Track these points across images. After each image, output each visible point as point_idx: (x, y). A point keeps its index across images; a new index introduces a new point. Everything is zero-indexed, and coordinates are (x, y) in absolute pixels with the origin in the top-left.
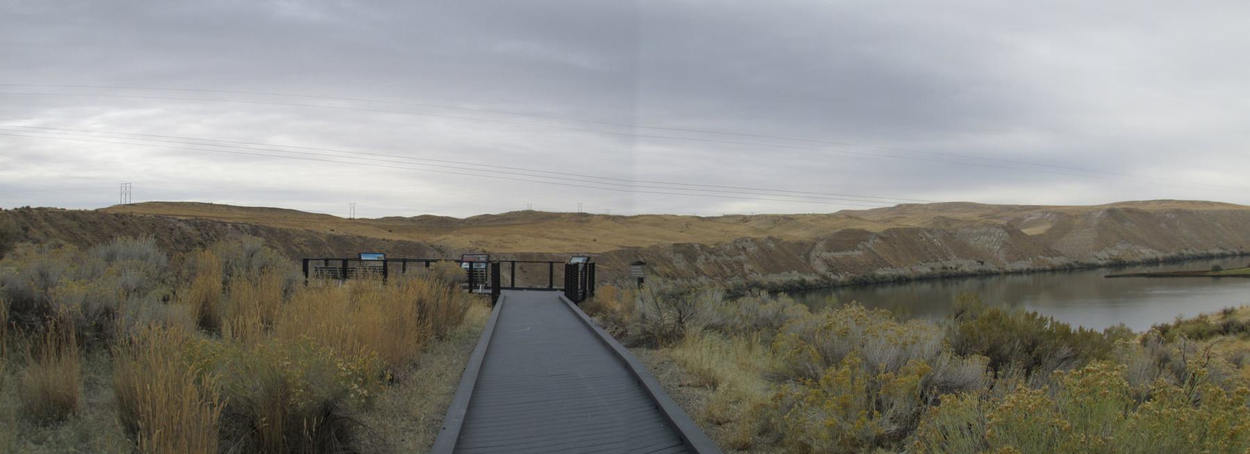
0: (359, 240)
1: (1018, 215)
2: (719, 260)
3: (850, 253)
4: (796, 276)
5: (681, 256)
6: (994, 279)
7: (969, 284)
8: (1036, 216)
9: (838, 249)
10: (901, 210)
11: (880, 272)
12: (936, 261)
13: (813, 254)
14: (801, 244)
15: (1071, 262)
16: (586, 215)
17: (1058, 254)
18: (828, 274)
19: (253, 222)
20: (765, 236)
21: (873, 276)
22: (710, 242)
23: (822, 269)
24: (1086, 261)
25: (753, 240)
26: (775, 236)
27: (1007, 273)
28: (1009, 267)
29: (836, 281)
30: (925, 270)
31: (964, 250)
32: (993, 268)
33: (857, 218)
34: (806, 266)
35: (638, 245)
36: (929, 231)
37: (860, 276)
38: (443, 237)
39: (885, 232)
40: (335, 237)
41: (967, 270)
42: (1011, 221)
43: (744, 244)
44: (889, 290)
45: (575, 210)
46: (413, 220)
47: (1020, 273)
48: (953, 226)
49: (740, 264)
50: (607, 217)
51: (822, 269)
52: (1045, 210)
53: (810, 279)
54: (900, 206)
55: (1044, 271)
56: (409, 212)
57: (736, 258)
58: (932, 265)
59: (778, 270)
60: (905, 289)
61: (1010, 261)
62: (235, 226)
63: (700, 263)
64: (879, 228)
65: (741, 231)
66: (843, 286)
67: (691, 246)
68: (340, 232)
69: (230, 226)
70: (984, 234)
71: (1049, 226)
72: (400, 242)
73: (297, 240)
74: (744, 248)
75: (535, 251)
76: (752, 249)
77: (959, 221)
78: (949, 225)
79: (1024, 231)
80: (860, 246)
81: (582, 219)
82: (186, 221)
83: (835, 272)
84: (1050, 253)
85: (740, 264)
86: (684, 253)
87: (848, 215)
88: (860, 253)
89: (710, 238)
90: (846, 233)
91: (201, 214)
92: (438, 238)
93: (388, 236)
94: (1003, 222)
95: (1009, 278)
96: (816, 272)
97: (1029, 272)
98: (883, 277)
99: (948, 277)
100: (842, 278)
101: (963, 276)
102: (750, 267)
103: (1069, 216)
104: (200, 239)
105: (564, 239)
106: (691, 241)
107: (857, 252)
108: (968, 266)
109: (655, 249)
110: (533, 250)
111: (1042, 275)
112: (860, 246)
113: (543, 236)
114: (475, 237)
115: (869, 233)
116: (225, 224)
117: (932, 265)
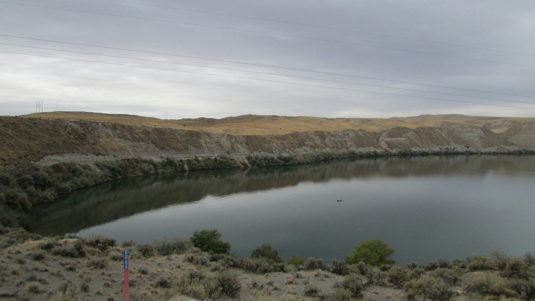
0: (168, 131)
1: (488, 122)
2: (336, 139)
3: (399, 139)
4: (372, 149)
5: (318, 137)
6: (474, 156)
7: (459, 158)
8: (499, 122)
9: (393, 137)
10: (423, 118)
11: (414, 149)
12: (443, 145)
13: (380, 138)
14: (375, 133)
15: (520, 149)
16: (276, 116)
17: (512, 145)
18: (388, 149)
19: (113, 122)
20: (358, 129)
21: (410, 151)
22: (332, 130)
23: (385, 146)
24: (530, 149)
25: (352, 130)
26: (363, 128)
27: (482, 154)
28: (483, 150)
29: (391, 153)
30: (436, 149)
31: (458, 140)
32: (474, 150)
33: (402, 121)
34: (377, 144)
35: (297, 131)
36: (440, 129)
37: (403, 151)
38: (209, 128)
39: (417, 128)
40: (156, 129)
41: (460, 150)
42: (485, 125)
43: (348, 132)
44: (417, 159)
45: (271, 114)
46: (195, 120)
47: (489, 154)
48: (453, 127)
49: (346, 142)
50: (286, 117)
51: (385, 146)
52: (505, 120)
53: (379, 151)
54: (422, 115)
55: (504, 154)
56: (194, 116)
57: (344, 139)
58: (441, 147)
59: (363, 146)
60: (425, 159)
61: (484, 147)
62: (103, 124)
63: (327, 141)
64: (413, 127)
65: (346, 126)
66: (395, 155)
67: (323, 132)
68: (159, 126)
69: (100, 124)
70: (470, 132)
71: (506, 129)
72: (189, 131)
73: (137, 131)
74: (348, 134)
75: (252, 134)
76: (352, 135)
77: (455, 124)
78: (450, 127)
79: (493, 131)
80: (404, 135)
81: (274, 118)
82: (75, 122)
83: (391, 148)
84: (507, 143)
85: (346, 142)
86: (320, 135)
87: (398, 120)
88: (404, 139)
89: (332, 128)
90: (397, 129)
91: (84, 118)
92: (207, 129)
93: (183, 128)
94: (481, 126)
95: (483, 156)
96: (382, 148)
97: (495, 154)
98: (415, 152)
99: (448, 154)
100: (394, 151)
101: (457, 154)
102: (350, 144)
103: (519, 123)
104: (83, 132)
105: (266, 128)
106: (322, 130)
107: (402, 139)
108: (460, 148)
109: (306, 133)
110: (252, 134)
111: (502, 156)
112: (404, 135)
113: (256, 127)
114: (225, 128)
115: (409, 129)
116: (97, 123)
117: (441, 147)
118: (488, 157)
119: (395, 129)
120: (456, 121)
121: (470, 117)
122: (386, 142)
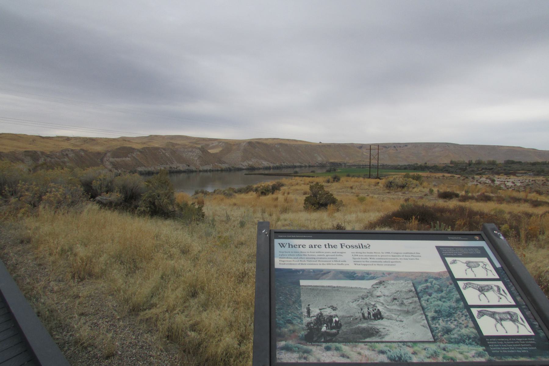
3: (124, 159)
6: (194, 174)
7: (182, 175)
8: (216, 143)
10: (152, 138)
13: (105, 159)
14: (99, 153)
17: (224, 163)
25: (72, 150)
26: (85, 149)
27: (200, 171)
42: (203, 145)
47: (206, 171)
48: (176, 147)
55: (218, 171)
64: (139, 147)
65: (66, 145)
67: (36, 152)
74: (67, 155)
76: (71, 155)
89: (48, 148)
94: (200, 146)
95: (201, 174)
97: (211, 171)
99: (172, 172)
101: (180, 172)
108: (182, 167)
118: (205, 174)
119: (119, 149)
120: (179, 142)
121: (194, 138)
122: (111, 163)
